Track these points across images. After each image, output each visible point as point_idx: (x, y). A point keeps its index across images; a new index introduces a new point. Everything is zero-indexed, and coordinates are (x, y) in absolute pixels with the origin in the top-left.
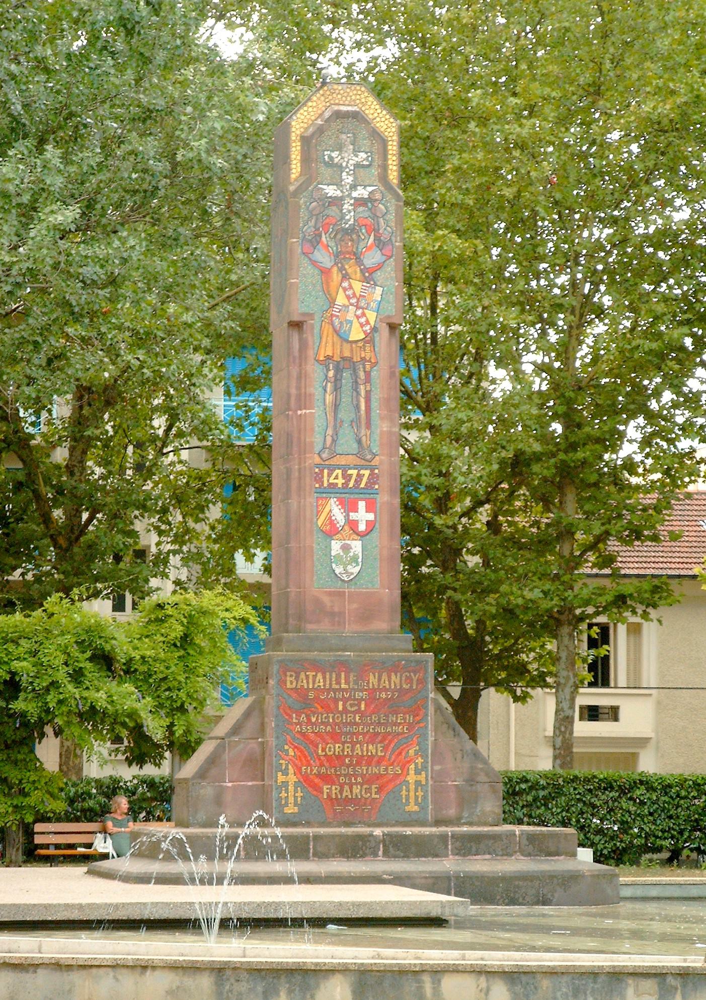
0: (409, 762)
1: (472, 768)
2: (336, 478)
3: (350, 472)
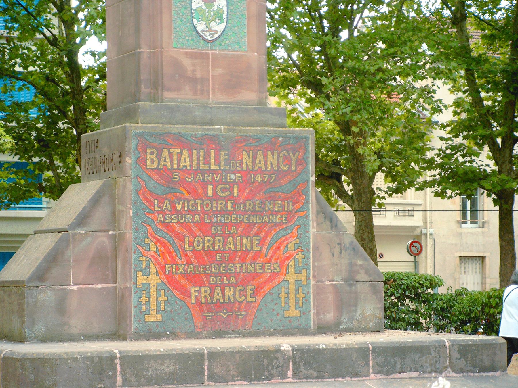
0: (288, 258)
1: (351, 265)
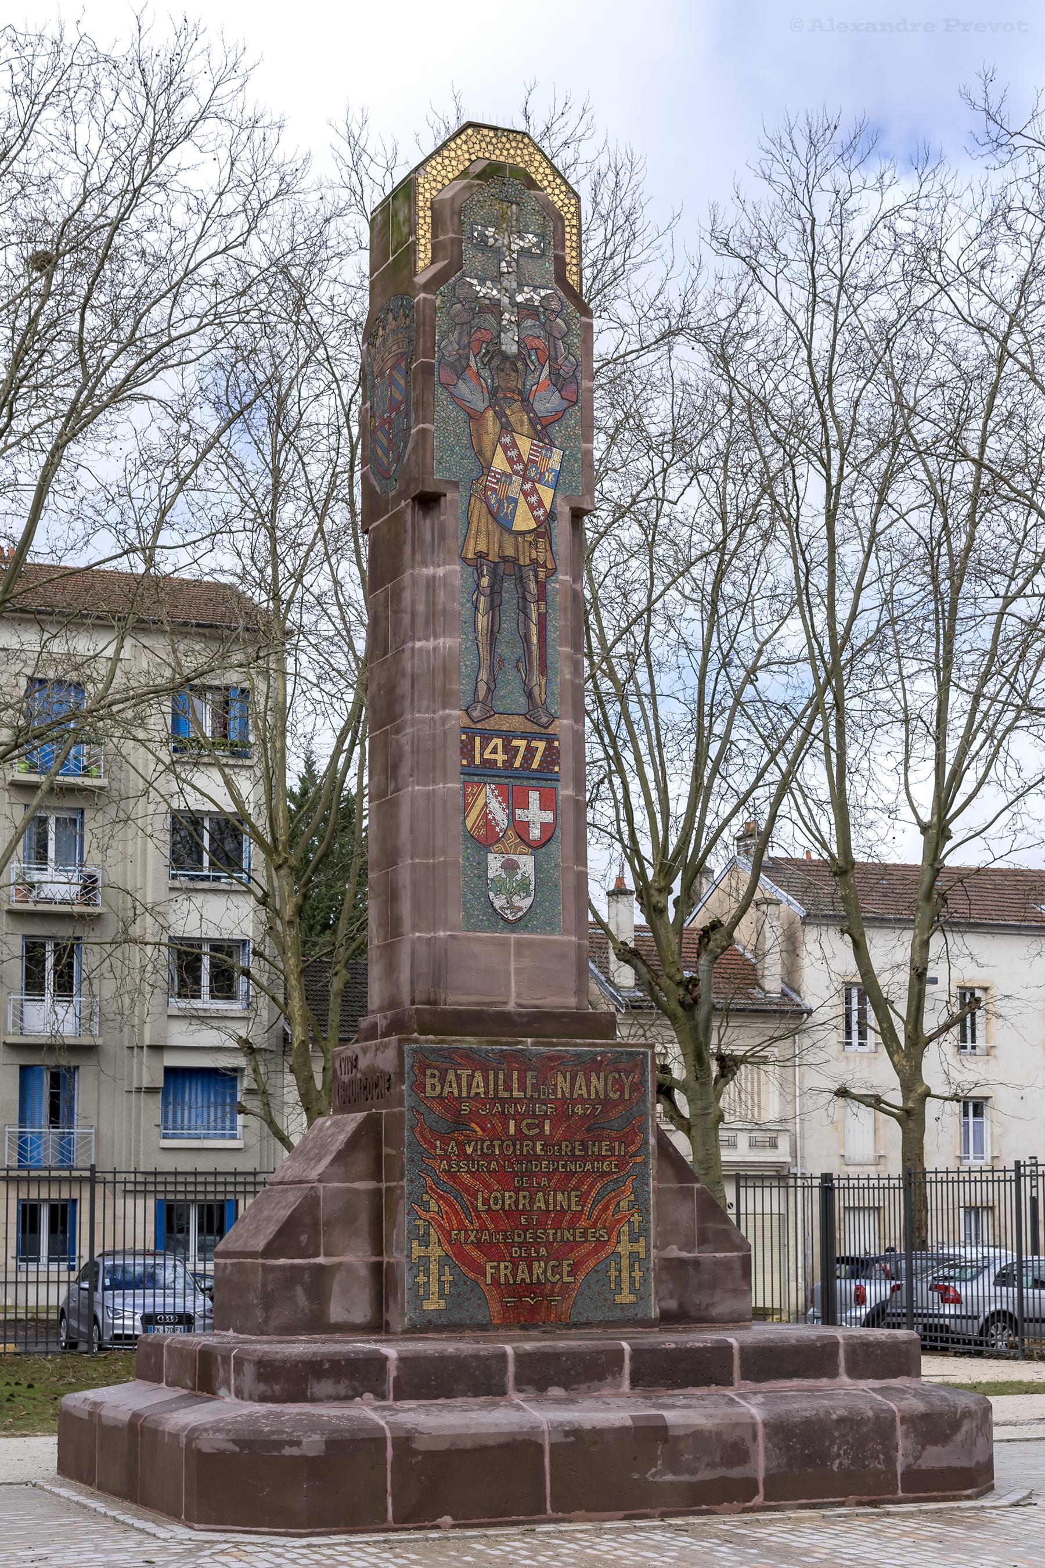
2: (495, 751)
3: (515, 743)
